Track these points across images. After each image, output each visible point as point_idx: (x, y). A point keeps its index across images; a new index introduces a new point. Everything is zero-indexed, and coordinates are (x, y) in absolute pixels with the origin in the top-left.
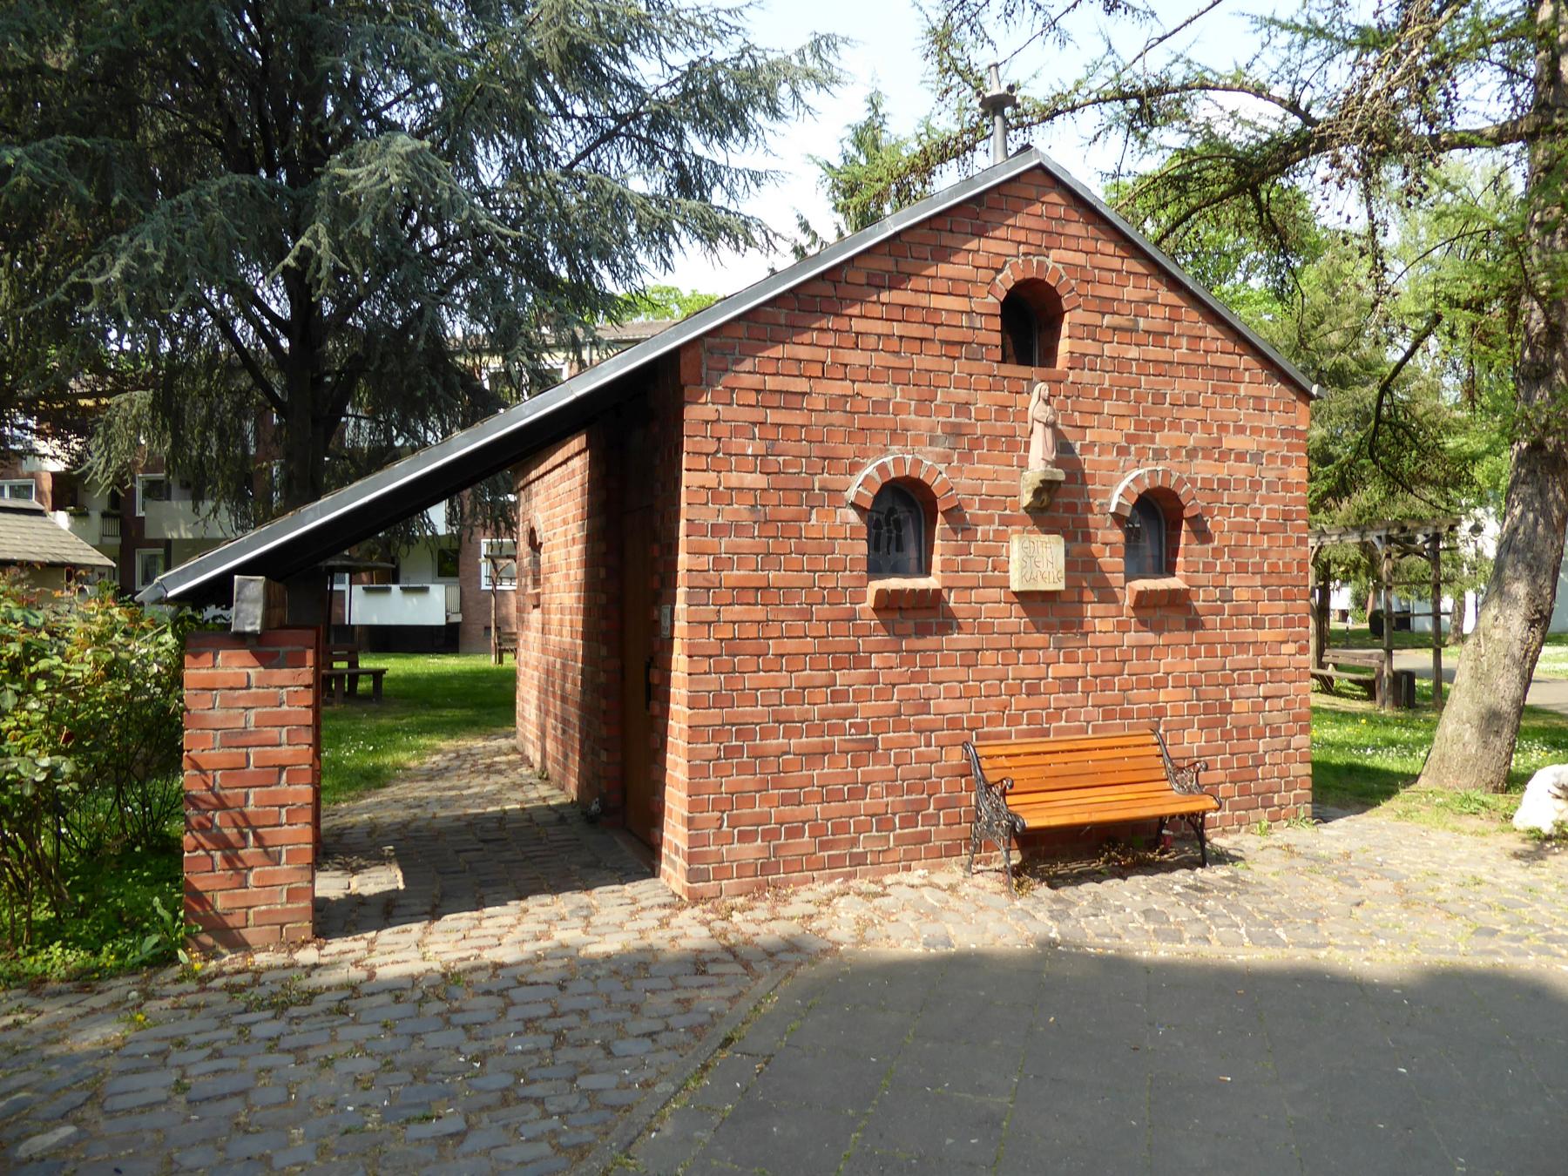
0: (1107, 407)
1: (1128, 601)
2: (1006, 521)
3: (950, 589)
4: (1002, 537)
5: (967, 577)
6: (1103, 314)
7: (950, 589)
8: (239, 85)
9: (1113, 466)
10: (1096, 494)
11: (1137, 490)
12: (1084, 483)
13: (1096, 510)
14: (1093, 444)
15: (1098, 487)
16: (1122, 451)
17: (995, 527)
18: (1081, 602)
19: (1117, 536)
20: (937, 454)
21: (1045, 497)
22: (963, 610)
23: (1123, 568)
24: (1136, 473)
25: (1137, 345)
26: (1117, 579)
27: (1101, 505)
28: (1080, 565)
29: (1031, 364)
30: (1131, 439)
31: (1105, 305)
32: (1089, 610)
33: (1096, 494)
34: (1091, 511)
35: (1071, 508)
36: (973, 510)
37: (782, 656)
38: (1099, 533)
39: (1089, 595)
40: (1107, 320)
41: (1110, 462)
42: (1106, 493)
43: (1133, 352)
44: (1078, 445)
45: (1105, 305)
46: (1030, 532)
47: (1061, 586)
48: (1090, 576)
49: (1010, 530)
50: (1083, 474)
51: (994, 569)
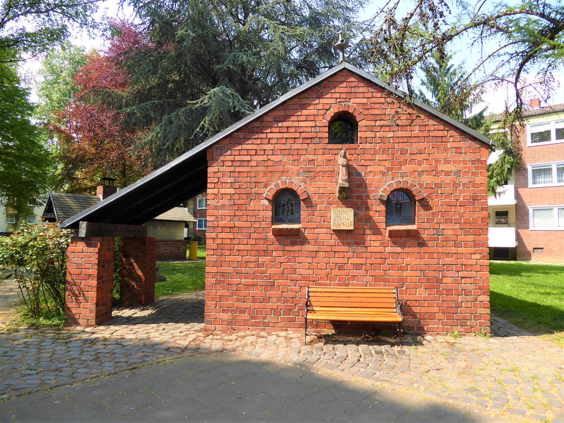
2: (330, 204)
3: (305, 228)
4: (327, 210)
5: (313, 225)
6: (376, 121)
7: (305, 228)
9: (380, 181)
11: (389, 190)
12: (366, 187)
13: (372, 198)
14: (371, 172)
15: (372, 189)
16: (383, 174)
19: (382, 208)
20: (300, 179)
21: (344, 193)
23: (385, 221)
26: (382, 226)
27: (374, 196)
28: (363, 220)
30: (389, 169)
32: (368, 238)
34: (370, 198)
35: (360, 197)
36: (315, 199)
37: (377, 211)
38: (373, 207)
39: (368, 232)
40: (378, 123)
41: (379, 179)
42: (376, 191)
43: (391, 134)
44: (363, 173)
46: (340, 207)
47: (352, 228)
48: (369, 224)
50: (366, 184)
51: (324, 221)
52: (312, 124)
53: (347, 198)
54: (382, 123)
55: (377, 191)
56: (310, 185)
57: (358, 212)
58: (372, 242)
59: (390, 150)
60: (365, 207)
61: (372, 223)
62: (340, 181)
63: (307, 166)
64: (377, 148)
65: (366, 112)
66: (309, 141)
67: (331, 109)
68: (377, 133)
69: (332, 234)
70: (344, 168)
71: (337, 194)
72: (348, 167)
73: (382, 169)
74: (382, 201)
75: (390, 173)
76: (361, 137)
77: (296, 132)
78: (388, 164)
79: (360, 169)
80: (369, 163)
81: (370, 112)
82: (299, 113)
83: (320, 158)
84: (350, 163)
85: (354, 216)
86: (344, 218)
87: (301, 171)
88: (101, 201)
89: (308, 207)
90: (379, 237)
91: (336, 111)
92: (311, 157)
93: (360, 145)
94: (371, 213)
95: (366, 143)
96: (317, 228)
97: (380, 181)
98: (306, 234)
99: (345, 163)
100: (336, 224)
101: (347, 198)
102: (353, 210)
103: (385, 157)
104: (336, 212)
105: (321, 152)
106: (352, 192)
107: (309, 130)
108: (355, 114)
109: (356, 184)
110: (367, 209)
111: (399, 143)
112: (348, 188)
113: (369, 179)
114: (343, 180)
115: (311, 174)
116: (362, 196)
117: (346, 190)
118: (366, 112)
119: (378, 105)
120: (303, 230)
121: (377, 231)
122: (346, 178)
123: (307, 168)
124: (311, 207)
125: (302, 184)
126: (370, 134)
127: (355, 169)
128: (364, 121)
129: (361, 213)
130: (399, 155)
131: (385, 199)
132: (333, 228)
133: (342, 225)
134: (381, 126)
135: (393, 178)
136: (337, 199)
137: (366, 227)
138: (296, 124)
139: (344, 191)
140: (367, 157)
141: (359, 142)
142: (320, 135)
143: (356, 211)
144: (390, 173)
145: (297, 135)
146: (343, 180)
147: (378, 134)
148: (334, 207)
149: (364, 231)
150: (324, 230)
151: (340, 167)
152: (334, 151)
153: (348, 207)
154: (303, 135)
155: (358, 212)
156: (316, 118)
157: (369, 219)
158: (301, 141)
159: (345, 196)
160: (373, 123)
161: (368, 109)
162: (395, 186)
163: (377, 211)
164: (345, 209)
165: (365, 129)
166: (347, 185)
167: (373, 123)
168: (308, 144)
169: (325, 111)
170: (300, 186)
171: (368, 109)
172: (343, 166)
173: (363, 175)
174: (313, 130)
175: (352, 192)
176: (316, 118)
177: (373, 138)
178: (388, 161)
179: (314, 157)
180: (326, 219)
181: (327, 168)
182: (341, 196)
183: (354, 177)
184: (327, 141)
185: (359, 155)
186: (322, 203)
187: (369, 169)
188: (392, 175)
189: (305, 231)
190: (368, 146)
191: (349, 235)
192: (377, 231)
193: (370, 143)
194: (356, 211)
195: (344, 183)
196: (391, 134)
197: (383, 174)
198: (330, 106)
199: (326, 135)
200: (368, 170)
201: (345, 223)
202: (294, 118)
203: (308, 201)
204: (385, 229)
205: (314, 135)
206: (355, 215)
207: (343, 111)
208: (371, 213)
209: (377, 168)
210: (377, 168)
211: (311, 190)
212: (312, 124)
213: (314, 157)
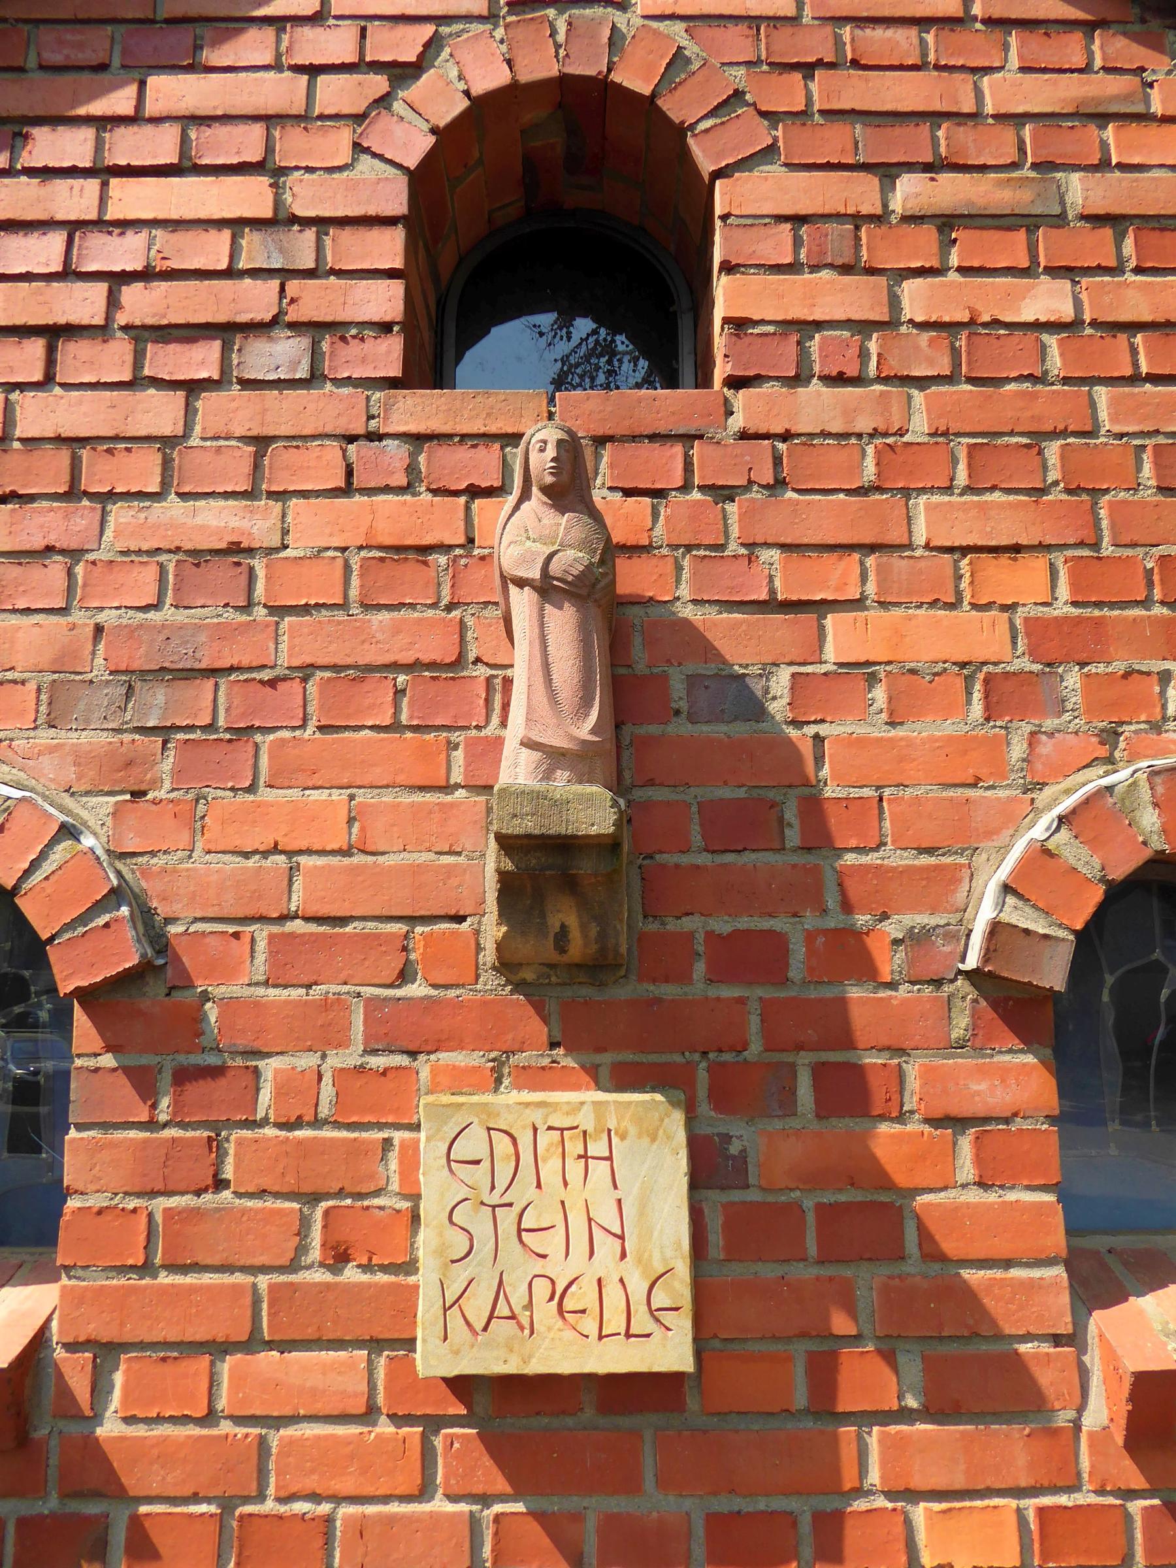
0: (925, 521)
1: (1102, 1412)
2: (408, 1035)
3: (105, 1352)
4: (375, 1102)
5: (201, 1297)
6: (888, 172)
7: (105, 1352)
8: (597, 342)
9: (971, 768)
10: (889, 890)
11: (1091, 865)
12: (819, 840)
13: (891, 963)
14: (862, 671)
15: (894, 858)
16: (1005, 695)
17: (350, 1057)
18: (824, 1405)
19: (1016, 1079)
20: (79, 758)
21: (564, 914)
22: (166, 1453)
23: (1057, 1240)
24: (1095, 780)
25: (1068, 272)
26: (1027, 1293)
27: (917, 939)
28: (791, 1234)
29: (678, 388)
30: (1055, 643)
31: (890, 143)
32: (874, 1456)
33: (889, 890)
34: (867, 971)
35: (754, 957)
36: (236, 984)
37: (958, 1123)
38: (913, 1070)
39: (866, 1379)
40: (909, 192)
41: (962, 745)
42: (941, 884)
43: (1047, 300)
44: (781, 681)
45: (890, 143)
46: (531, 1078)
47: (671, 1351)
48: (868, 1280)
49: (424, 1067)
50: (813, 806)
51: (339, 1257)
52: (250, 197)
53: (600, 967)
54: (951, 192)
55: (948, 878)
56: (194, 823)
57: (743, 1135)
58: (920, 1512)
59: (1053, 450)
60: (819, 1071)
61: (913, 1267)
62: (517, 769)
63: (167, 614)
64: (919, 427)
65: (788, 94)
66: (202, 360)
67: (444, 69)
68: (910, 289)
69: (433, 1423)
70: (563, 622)
71: (492, 930)
72: (598, 596)
73: (988, 639)
74: (1010, 1003)
75: (1073, 679)
76: (738, 325)
77: (68, 273)
78: (1042, 591)
79: (739, 642)
80: (837, 577)
81: (822, 90)
82: (121, 101)
83: (314, 525)
84: (634, 578)
85: (696, 1183)
86: (567, 1225)
87: (99, 669)
88: (398, 1136)
89: (144, 1083)
90: (1012, 1448)
91: (490, 77)
92: (217, 521)
93: (740, 399)
94: (889, 1141)
95: (798, 380)
96: (252, 1343)
97: (971, 768)
98: (110, 1428)
99: (571, 561)
100: (477, 1306)
101: (600, 967)
102: (676, 1123)
103: (1003, 517)
104: (472, 1145)
105: (323, 466)
106: (657, 892)
107: (213, 251)
108: (675, 108)
109: (710, 812)
110: (849, 1094)
111: (1135, 379)
112: (609, 846)
113: (845, 749)
114: (554, 757)
115: (191, 715)
116: (777, 943)
117: (585, 867)
118: (788, 94)
119: (904, 41)
120: (76, 1372)
121: (977, 1379)
122: (585, 729)
123: (168, 632)
124: (182, 1077)
125: (96, 811)
126: (836, 297)
127: (692, 640)
128: (774, 170)
129: (776, 1146)
130: (1148, 495)
131: (1053, 973)
132: (434, 1359)
133: (545, 1312)
134: (947, 223)
135: (1110, 736)
136: (490, 982)
137: (841, 1324)
138: (75, 200)
139: (570, 885)
140: (824, 519)
141: (720, 373)
142: (315, 300)
143: (715, 1123)
144: (1073, 679)
145: (83, 303)
146: (554, 757)
147: (916, 299)
148: (459, 1081)
149: (823, 1374)
150: (337, 1372)
151: (522, 602)
152: (462, 454)
153: (626, 1079)
154: (139, 303)
155: (743, 1135)
156: (293, 146)
157: (873, 1221)
158: (114, 359)
159: (577, 948)
160: (862, 193)
161: (808, 69)
162: (1149, 819)
163: (958, 1123)
164: (584, 1103)
165: (778, 245)
166: (592, 811)
167: (862, 193)
168: (193, 388)
169: (379, 83)
170: (68, 832)
171: (808, 69)
172: (547, 589)
173: (778, 708)
174: (257, 250)
175: (657, 892)
176: (293, 146)
177: (864, 327)
178: (1038, 564)
179: (256, 523)
180: (363, 1230)
181: (384, 636)
182: (532, 948)
183: (680, 728)
184: (387, 356)
185: (723, 493)
186: (323, 1029)
187: (841, 640)
188: (1091, 709)
189: (99, 1388)
190: (816, 407)
191: (647, 1423)
192: (977, 1379)
193: (839, 379)
194: (715, 1123)
195: (562, 783)
196: (1047, 300)
197: (1005, 695)
198: (433, 45)
199: (385, 300)
200: (831, 653)
201: (582, 1296)
202: (68, 146)
203: (151, 1000)
204: (1074, 1339)
205: (256, 300)
206: (708, 1168)
207: (564, 82)
208: (889, 1141)
209: (932, 637)
210: (932, 637)
211: (194, 878)
212: (250, 197)
213: (256, 523)
